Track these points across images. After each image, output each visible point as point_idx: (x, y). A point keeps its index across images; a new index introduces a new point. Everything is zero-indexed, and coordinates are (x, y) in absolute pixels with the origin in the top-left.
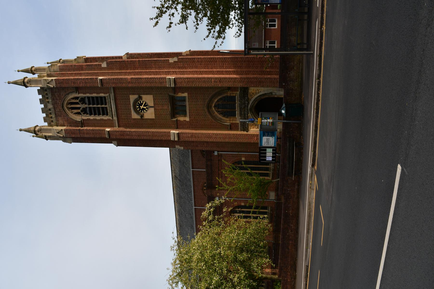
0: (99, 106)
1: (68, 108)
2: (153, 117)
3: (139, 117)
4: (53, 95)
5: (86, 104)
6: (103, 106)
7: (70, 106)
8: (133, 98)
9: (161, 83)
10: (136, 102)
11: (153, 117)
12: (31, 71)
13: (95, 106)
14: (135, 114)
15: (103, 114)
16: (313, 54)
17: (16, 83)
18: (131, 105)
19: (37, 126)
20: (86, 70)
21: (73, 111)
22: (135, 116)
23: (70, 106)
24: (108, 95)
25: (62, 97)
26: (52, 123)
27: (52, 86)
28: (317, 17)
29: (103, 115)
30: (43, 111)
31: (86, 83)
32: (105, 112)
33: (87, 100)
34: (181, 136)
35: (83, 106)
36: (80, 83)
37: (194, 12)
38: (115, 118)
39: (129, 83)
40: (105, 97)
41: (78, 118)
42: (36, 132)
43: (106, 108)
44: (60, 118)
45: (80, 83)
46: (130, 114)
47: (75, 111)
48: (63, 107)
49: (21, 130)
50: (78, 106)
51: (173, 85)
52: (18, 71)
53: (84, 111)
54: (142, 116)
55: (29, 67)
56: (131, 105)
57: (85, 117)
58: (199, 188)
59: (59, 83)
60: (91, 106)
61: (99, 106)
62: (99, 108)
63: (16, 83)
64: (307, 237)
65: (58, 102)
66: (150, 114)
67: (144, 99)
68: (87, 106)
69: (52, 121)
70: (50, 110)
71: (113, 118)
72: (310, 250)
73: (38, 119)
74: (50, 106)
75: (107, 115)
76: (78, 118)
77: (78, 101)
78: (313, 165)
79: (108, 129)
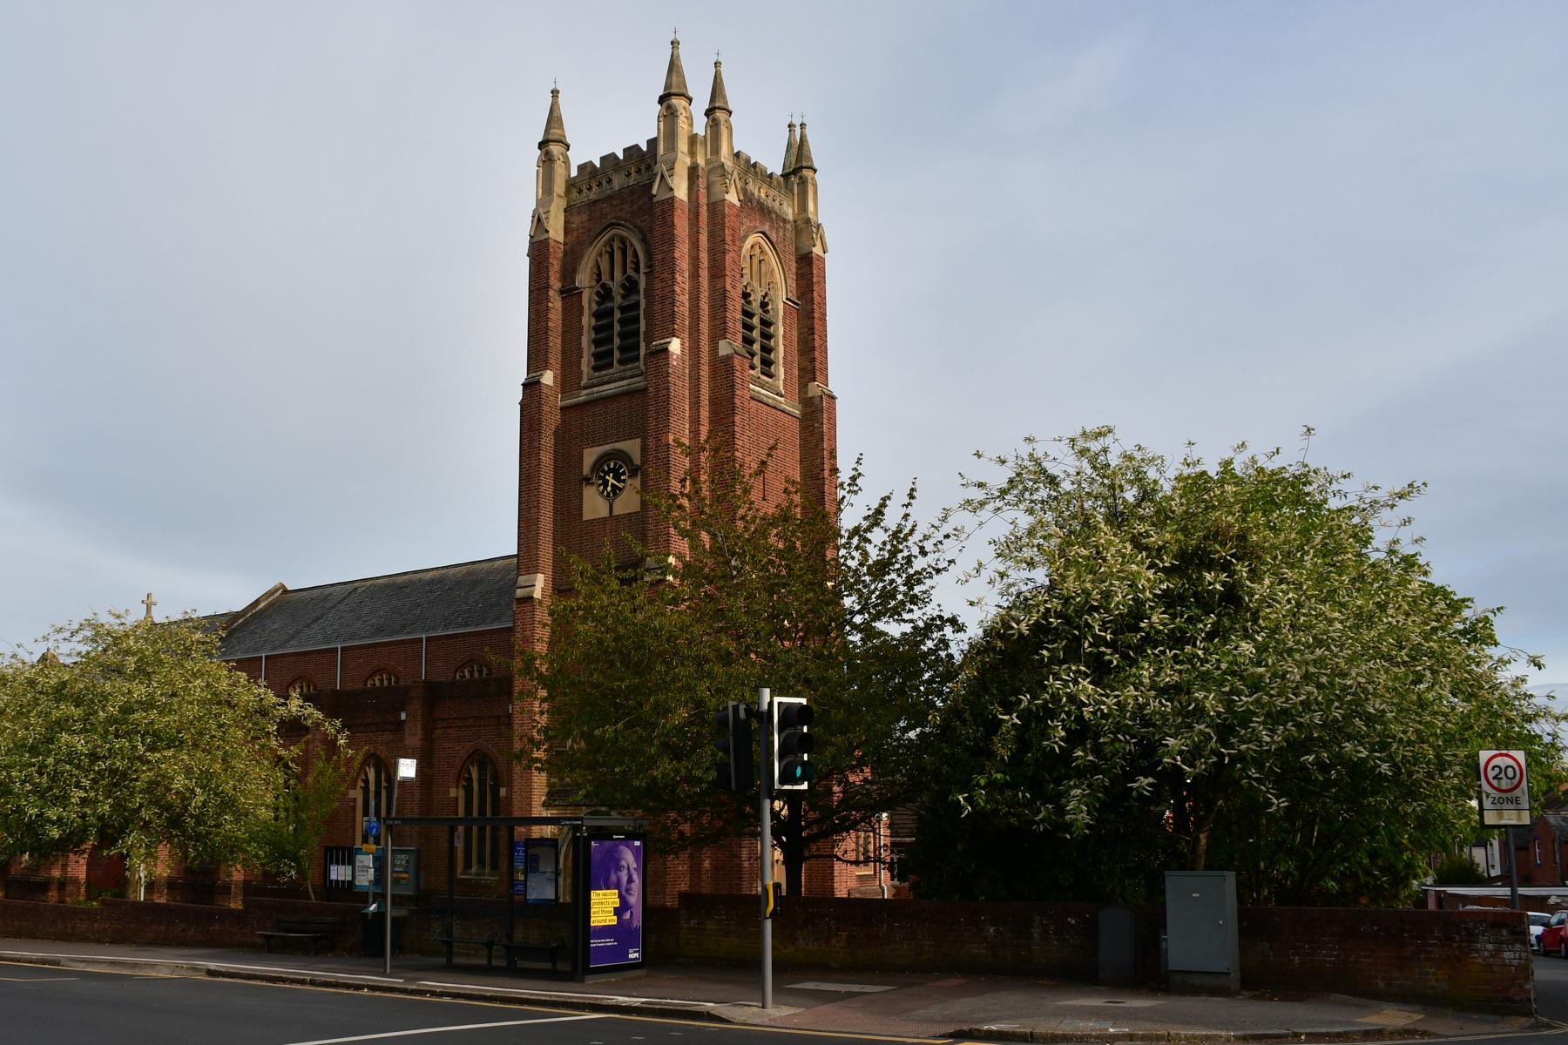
0: (617, 341)
1: (612, 239)
2: (588, 515)
3: (586, 470)
4: (632, 190)
5: (624, 297)
6: (617, 355)
7: (616, 245)
8: (632, 447)
9: (656, 540)
10: (623, 456)
11: (588, 515)
12: (717, 108)
13: (617, 328)
14: (594, 458)
15: (596, 356)
16: (384, 974)
17: (674, 66)
18: (617, 445)
19: (568, 147)
20: (712, 288)
21: (606, 257)
22: (590, 456)
23: (616, 245)
24: (643, 367)
25: (638, 222)
26: (574, 194)
27: (654, 191)
28: (407, 980)
29: (594, 355)
30: (608, 159)
31: (663, 298)
32: (602, 360)
33: (632, 299)
34: (527, 608)
35: (617, 292)
36: (662, 280)
37: (904, 634)
38: (583, 396)
39: (658, 439)
40: (637, 359)
41: (584, 278)
42: (551, 143)
43: (611, 365)
44: (585, 217)
45: (662, 280)
46: (594, 444)
47: (605, 266)
48: (612, 225)
49: (675, 44)
50: (618, 274)
51: (519, 593)
52: (717, 64)
53: (605, 294)
54: (588, 481)
55: (733, 98)
56: (617, 445)
57: (588, 300)
58: (376, 666)
59: (663, 212)
60: (617, 315)
61: (617, 341)
62: (612, 340)
63: (674, 66)
64: (103, 962)
65: (627, 207)
66: (594, 504)
67: (629, 482)
68: (618, 300)
69: (580, 191)
70: (610, 181)
71: (585, 388)
72: (81, 967)
73: (589, 145)
74: (618, 181)
75: (595, 369)
76: (584, 278)
77: (630, 272)
78: (211, 973)
79: (675, 346)
